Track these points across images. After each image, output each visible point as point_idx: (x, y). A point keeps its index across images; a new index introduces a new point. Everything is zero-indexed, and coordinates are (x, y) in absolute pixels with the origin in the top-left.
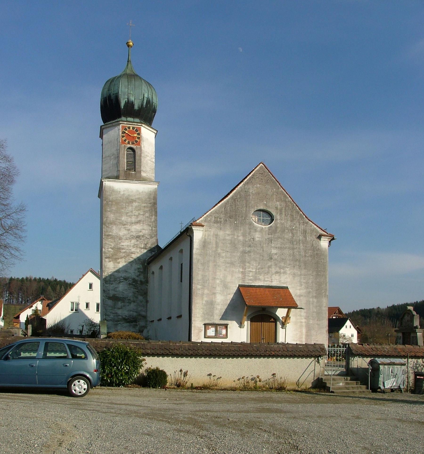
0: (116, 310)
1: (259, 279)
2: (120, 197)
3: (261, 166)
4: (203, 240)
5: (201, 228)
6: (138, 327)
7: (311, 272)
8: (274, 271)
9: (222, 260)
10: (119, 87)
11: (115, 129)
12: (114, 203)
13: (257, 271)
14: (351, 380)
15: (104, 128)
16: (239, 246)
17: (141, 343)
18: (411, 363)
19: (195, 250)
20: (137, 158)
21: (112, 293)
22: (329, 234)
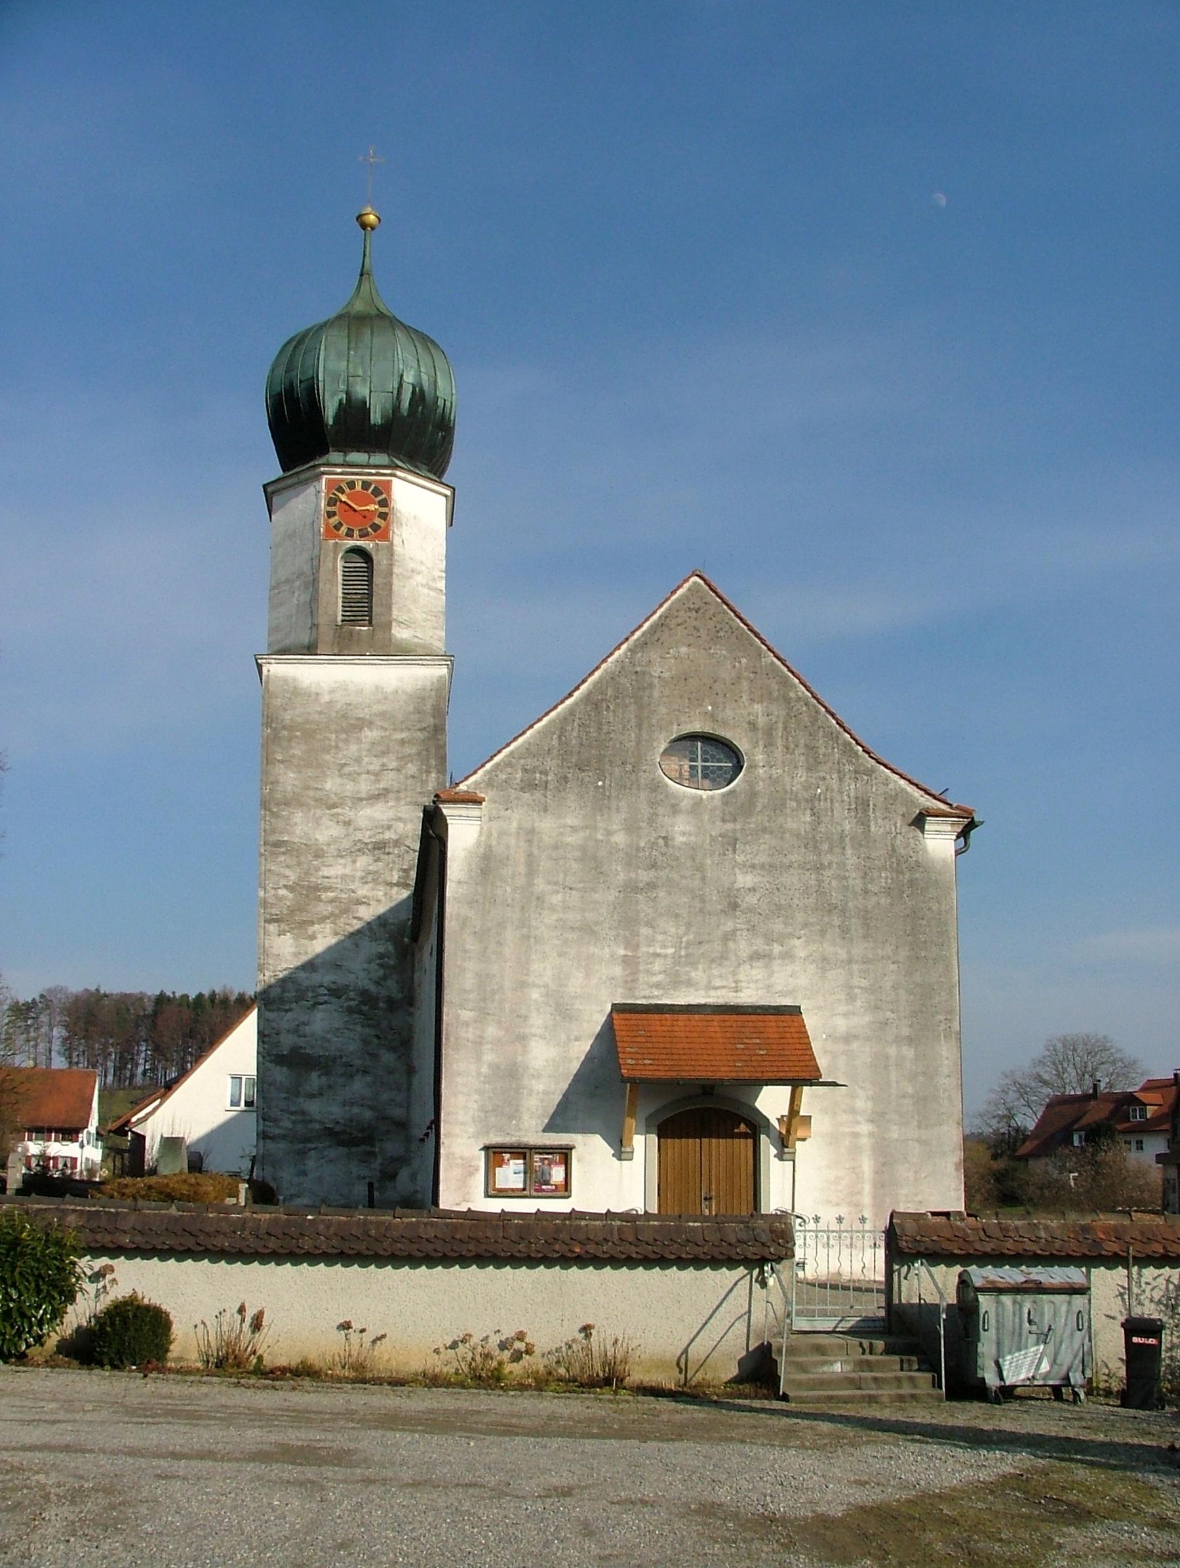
0: (301, 1100)
1: (690, 983)
2: (320, 713)
3: (695, 583)
4: (482, 850)
5: (473, 811)
6: (379, 1161)
7: (889, 950)
8: (747, 950)
9: (550, 918)
10: (318, 359)
11: (308, 491)
12: (298, 733)
13: (683, 953)
14: (888, 1351)
15: (273, 493)
16: (613, 868)
17: (107, 1210)
18: (1154, 1284)
19: (454, 885)
20: (378, 580)
21: (287, 1042)
22: (957, 808)
